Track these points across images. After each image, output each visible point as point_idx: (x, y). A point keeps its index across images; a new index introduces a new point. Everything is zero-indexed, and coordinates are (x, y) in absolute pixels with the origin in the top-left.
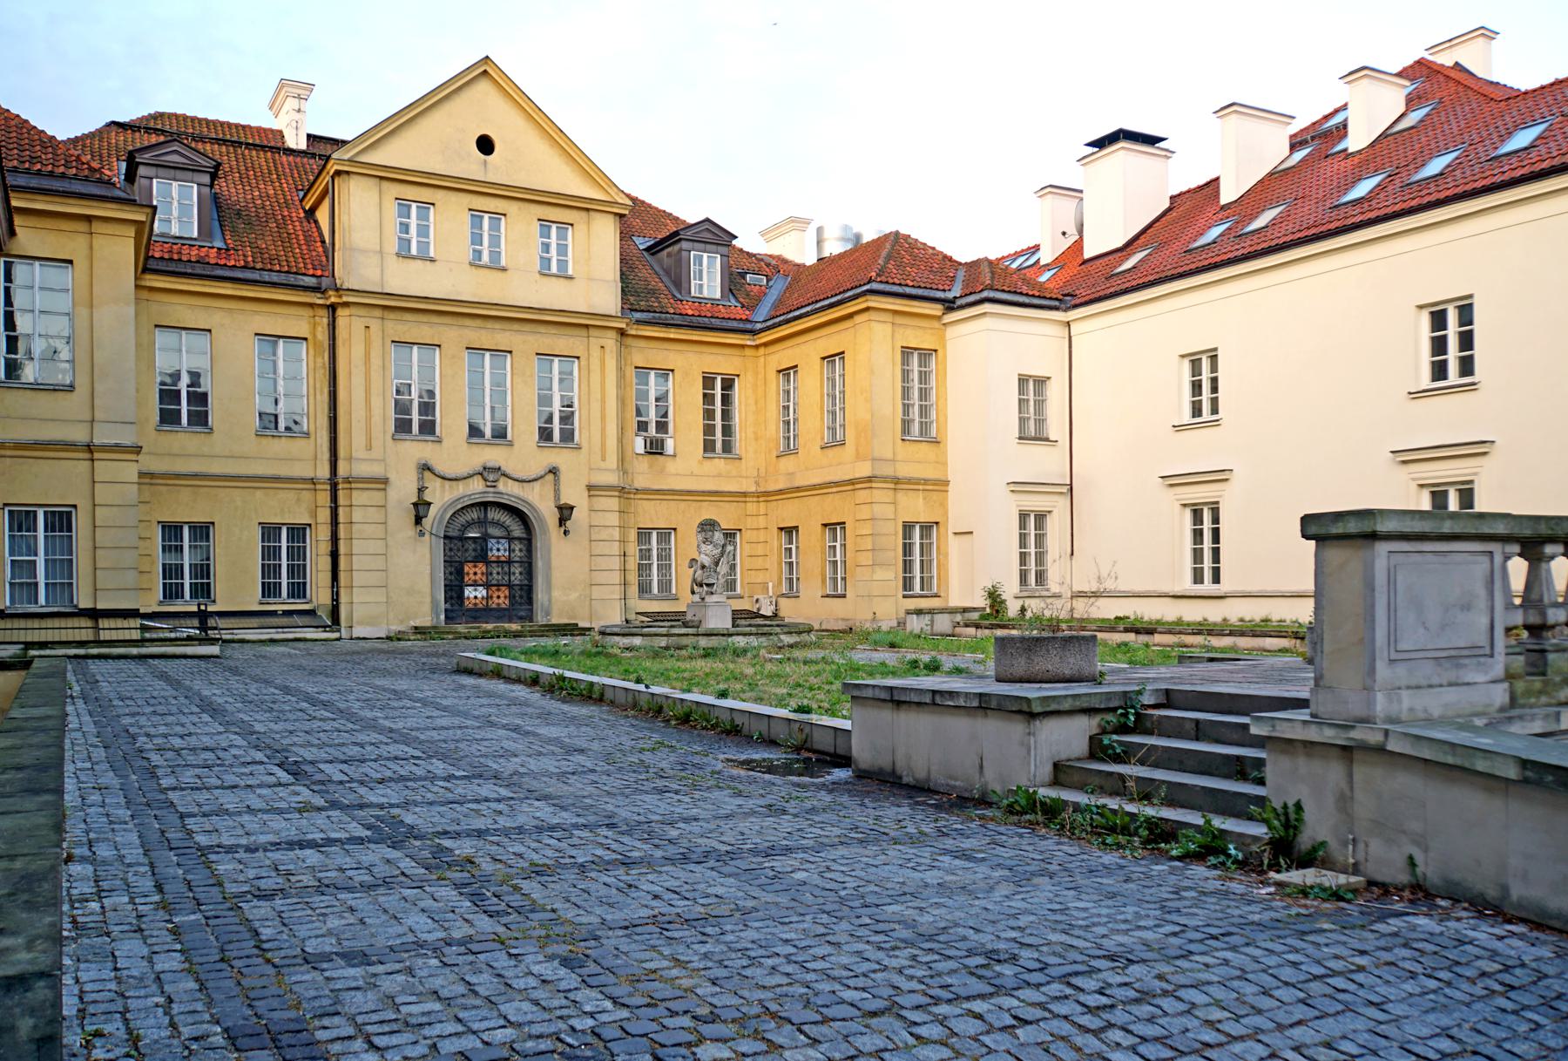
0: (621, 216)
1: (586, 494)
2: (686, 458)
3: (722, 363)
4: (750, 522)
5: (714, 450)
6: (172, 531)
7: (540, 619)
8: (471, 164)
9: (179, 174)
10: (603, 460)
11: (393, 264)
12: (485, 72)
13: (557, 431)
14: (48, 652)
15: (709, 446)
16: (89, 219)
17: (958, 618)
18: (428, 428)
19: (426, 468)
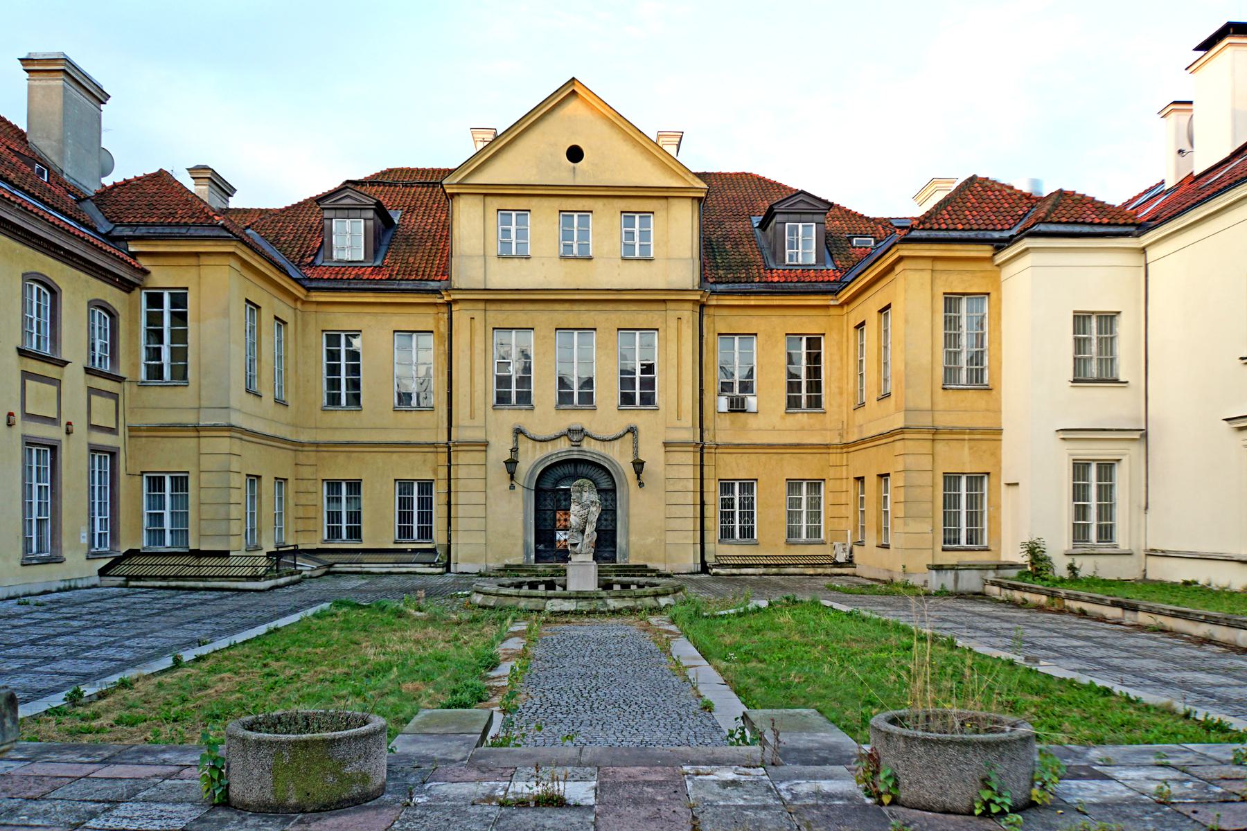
0: (700, 199)
1: (663, 450)
2: (768, 412)
3: (809, 324)
4: (832, 473)
5: (798, 405)
6: (334, 486)
7: (620, 561)
8: (563, 173)
9: (352, 213)
10: (679, 418)
11: (495, 266)
12: (574, 92)
13: (638, 390)
14: (142, 583)
15: (793, 403)
16: (197, 254)
17: (991, 575)
18: (525, 398)
19: (519, 432)
